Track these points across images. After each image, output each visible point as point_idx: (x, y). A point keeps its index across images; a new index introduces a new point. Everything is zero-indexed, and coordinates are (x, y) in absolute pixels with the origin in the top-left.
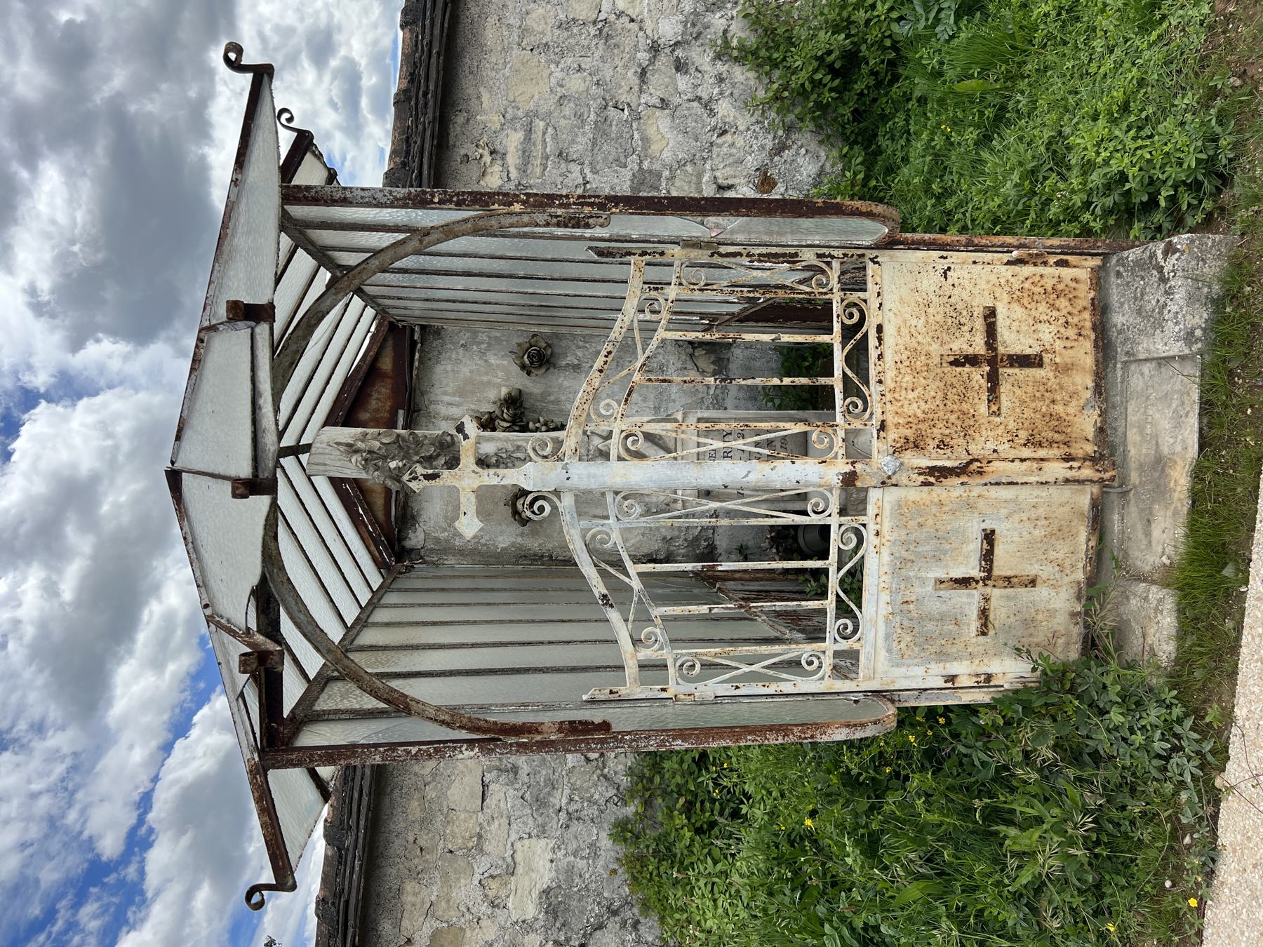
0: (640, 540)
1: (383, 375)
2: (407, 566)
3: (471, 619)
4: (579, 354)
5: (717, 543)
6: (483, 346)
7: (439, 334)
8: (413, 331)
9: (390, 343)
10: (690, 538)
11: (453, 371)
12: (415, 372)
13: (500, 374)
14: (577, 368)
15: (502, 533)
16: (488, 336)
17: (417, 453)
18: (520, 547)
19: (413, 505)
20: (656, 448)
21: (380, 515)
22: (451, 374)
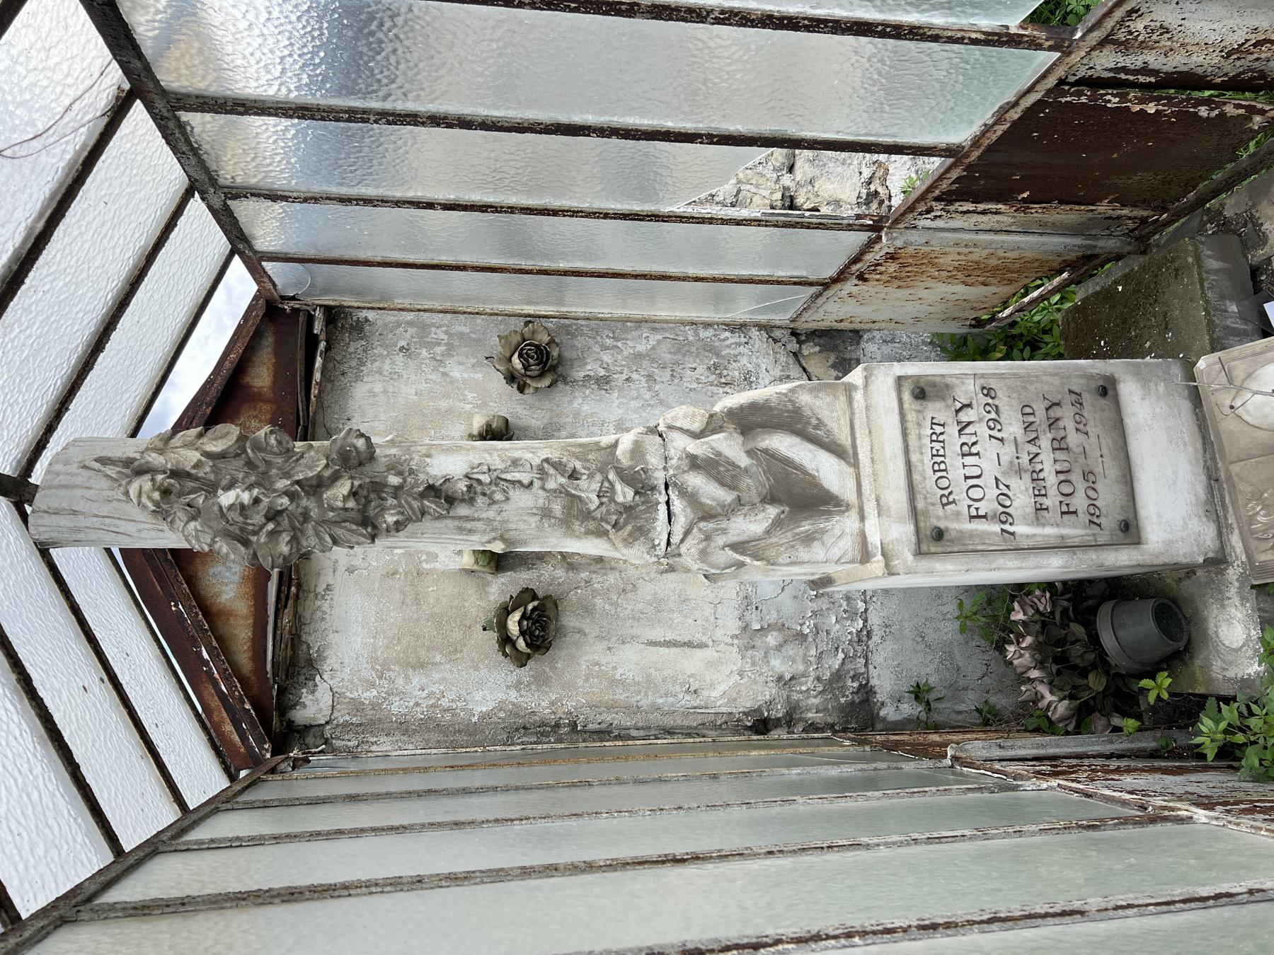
0: (736, 685)
1: (255, 398)
2: (295, 760)
3: (407, 870)
4: (607, 358)
5: (874, 682)
6: (439, 350)
7: (361, 330)
8: (310, 319)
9: (268, 343)
10: (827, 676)
11: (385, 392)
12: (314, 391)
13: (470, 396)
14: (603, 382)
15: (480, 684)
16: (446, 333)
17: (287, 475)
18: (515, 711)
19: (310, 639)
20: (811, 447)
21: (244, 658)
22: (382, 399)
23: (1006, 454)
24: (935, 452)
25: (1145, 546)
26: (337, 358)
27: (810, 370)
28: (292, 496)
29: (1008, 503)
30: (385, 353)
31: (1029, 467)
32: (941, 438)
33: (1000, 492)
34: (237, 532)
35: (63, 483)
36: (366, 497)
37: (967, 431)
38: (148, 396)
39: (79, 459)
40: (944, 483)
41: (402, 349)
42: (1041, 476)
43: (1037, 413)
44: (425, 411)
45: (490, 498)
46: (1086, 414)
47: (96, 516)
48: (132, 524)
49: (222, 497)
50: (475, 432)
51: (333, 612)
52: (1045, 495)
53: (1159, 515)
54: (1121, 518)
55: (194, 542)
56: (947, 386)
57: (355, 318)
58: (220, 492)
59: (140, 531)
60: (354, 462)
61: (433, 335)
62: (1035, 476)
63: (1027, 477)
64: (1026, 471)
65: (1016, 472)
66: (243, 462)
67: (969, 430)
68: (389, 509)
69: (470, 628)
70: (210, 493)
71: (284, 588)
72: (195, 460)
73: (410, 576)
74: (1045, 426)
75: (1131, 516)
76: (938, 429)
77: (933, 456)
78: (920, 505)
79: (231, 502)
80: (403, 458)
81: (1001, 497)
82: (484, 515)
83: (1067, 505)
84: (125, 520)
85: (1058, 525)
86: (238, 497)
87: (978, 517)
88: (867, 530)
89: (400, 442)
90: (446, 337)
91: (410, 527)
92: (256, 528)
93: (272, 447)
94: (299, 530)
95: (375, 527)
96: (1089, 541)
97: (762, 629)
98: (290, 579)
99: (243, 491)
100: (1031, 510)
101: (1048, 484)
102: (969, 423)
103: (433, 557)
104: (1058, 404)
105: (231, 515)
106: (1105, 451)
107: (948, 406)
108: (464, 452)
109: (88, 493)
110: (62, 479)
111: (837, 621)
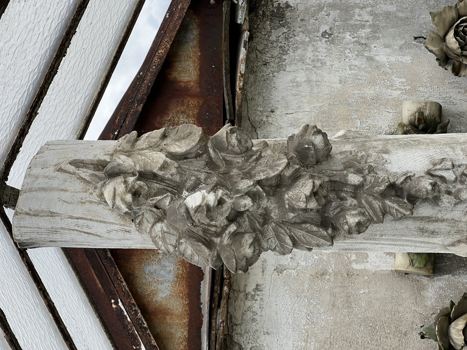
6: (363, 33)
12: (239, 83)
13: (398, 81)
16: (371, 13)
17: (248, 175)
26: (259, 48)
28: (254, 196)
30: (308, 39)
34: (201, 233)
35: (42, 186)
36: (325, 197)
38: (95, 97)
39: (55, 163)
41: (324, 34)
44: (350, 101)
45: (457, 197)
47: (71, 217)
48: (103, 225)
49: (188, 199)
50: (406, 121)
51: (263, 313)
55: (160, 243)
57: (276, 4)
58: (185, 193)
59: (109, 232)
60: (312, 160)
61: (357, 17)
66: (203, 162)
68: (349, 210)
69: (405, 334)
70: (174, 194)
71: (217, 288)
72: (161, 162)
73: (339, 277)
79: (198, 203)
80: (359, 155)
82: (449, 216)
84: (97, 221)
86: (204, 198)
89: (354, 138)
90: (370, 18)
91: (372, 228)
92: (219, 230)
93: (234, 147)
94: (260, 231)
95: (335, 229)
98: (222, 279)
99: (209, 192)
103: (363, 258)
105: (197, 218)
108: (423, 147)
109: (64, 196)
110: (41, 182)
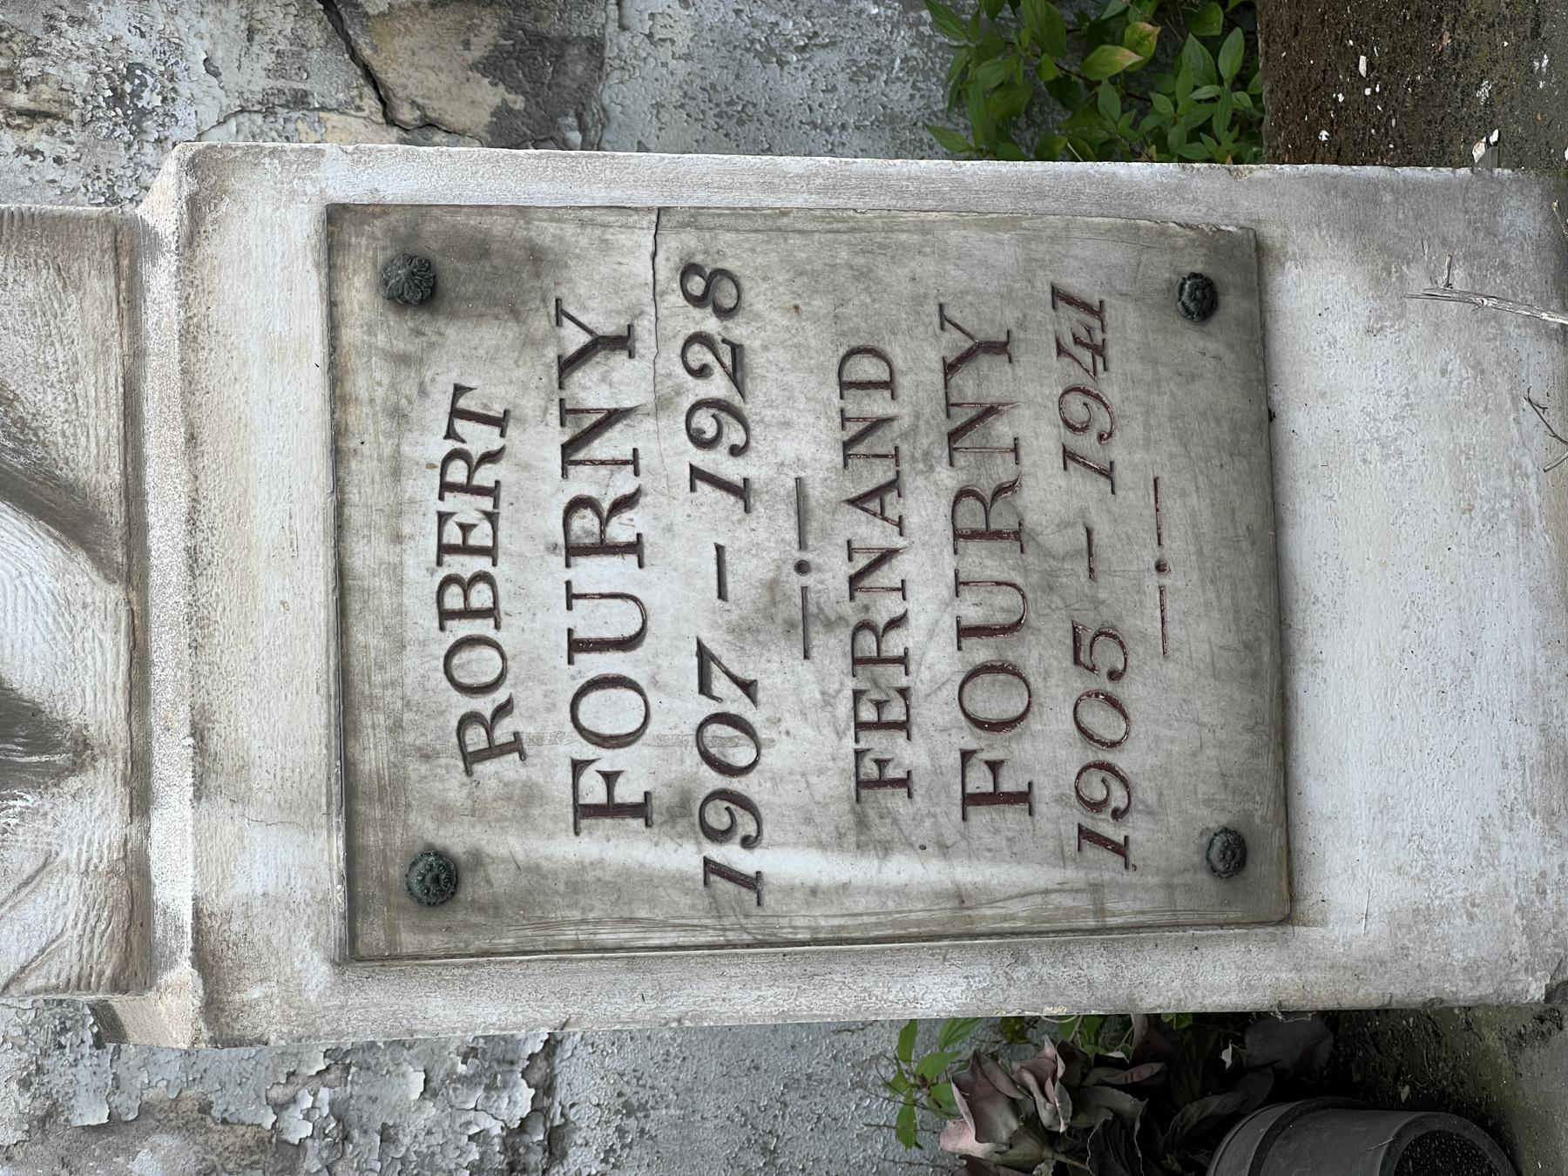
23: (755, 548)
24: (453, 535)
25: (1314, 933)
27: (389, 77)
29: (741, 755)
31: (847, 608)
32: (485, 477)
33: (712, 708)
37: (600, 448)
40: (482, 664)
42: (895, 644)
43: (905, 383)
46: (1112, 393)
52: (903, 726)
53: (1384, 807)
54: (1224, 820)
56: (538, 258)
62: (868, 643)
63: (832, 649)
64: (829, 625)
65: (790, 626)
67: (606, 446)
74: (932, 440)
75: (1261, 811)
76: (479, 438)
77: (444, 549)
78: (373, 756)
81: (715, 729)
83: (994, 766)
85: (944, 849)
87: (612, 810)
88: (154, 854)
96: (1069, 913)
97: (114, 1123)
100: (836, 785)
101: (920, 680)
102: (612, 417)
104: (1000, 348)
106: (1177, 547)
107: (530, 343)
111: (429, 1091)
